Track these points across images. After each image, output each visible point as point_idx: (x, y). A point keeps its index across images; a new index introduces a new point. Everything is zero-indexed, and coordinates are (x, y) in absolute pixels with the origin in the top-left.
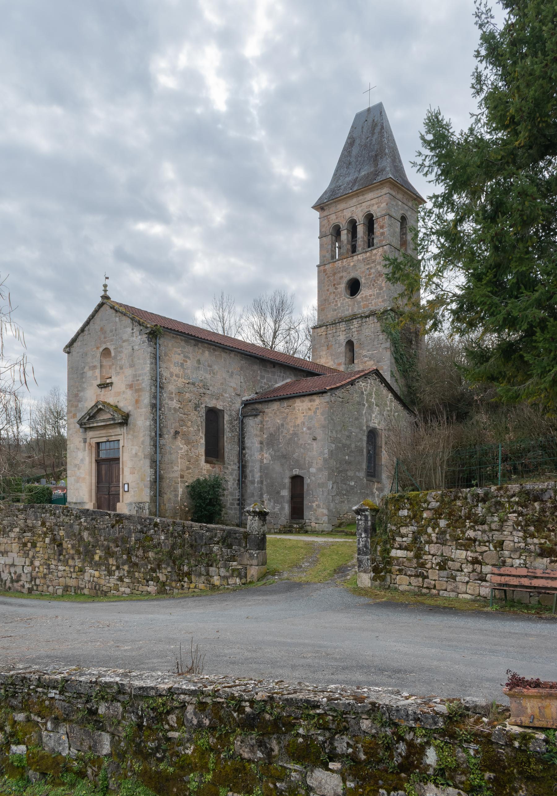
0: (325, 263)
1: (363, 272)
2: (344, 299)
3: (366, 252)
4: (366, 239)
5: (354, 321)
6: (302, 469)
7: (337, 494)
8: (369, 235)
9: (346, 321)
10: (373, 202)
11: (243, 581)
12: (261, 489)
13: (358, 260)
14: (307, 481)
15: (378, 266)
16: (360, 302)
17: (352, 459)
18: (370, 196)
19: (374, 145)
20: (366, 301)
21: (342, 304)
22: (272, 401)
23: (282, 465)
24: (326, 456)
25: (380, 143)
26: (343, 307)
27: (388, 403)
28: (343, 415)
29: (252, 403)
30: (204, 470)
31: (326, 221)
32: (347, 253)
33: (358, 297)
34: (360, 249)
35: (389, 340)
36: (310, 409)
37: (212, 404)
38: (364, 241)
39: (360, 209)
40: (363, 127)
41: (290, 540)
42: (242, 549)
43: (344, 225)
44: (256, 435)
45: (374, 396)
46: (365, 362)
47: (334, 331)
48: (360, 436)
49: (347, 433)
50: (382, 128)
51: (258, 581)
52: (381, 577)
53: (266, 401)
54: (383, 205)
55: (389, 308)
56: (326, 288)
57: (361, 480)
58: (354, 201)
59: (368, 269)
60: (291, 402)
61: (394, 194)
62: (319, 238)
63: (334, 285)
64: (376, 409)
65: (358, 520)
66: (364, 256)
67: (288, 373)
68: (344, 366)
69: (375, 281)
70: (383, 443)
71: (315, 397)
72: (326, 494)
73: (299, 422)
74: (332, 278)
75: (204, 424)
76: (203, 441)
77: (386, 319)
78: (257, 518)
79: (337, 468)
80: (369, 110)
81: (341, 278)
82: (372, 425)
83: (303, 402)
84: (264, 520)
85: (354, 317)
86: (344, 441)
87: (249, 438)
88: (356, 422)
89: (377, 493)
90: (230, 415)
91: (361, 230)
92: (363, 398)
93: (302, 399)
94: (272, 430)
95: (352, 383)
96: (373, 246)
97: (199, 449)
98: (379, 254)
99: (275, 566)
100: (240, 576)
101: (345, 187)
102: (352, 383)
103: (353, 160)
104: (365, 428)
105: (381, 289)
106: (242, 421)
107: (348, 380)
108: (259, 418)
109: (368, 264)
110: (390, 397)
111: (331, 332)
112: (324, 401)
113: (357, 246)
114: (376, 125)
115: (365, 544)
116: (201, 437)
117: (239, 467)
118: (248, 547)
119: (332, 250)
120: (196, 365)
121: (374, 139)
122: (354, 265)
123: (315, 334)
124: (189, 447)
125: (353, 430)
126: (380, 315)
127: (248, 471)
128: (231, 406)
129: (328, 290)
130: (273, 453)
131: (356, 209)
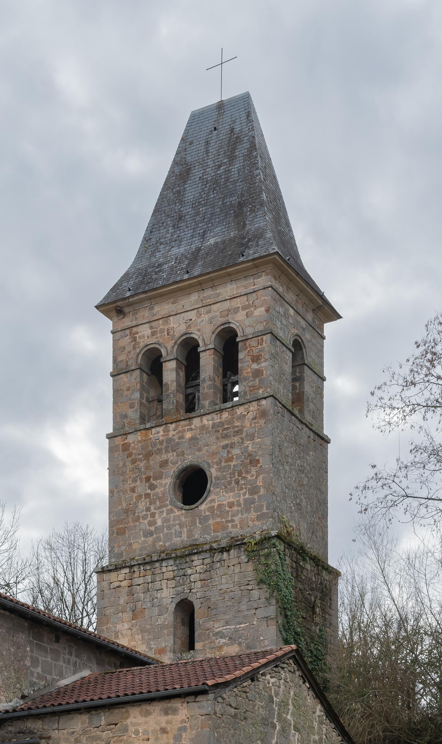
0: (127, 429)
1: (214, 454)
2: (171, 511)
3: (221, 410)
4: (218, 383)
5: (195, 557)
8: (224, 376)
9: (176, 558)
10: (237, 303)
13: (203, 427)
15: (247, 443)
16: (206, 519)
18: (229, 289)
19: (235, 182)
20: (221, 516)
21: (166, 520)
22: (68, 712)
26: (169, 528)
27: (316, 725)
29: (19, 718)
31: (128, 339)
32: (177, 410)
33: (203, 507)
34: (206, 403)
35: (274, 601)
36: (164, 731)
38: (215, 387)
39: (206, 317)
43: (169, 349)
45: (291, 707)
46: (220, 648)
50: (253, 147)
53: (53, 714)
54: (260, 311)
55: (274, 533)
56: (130, 484)
59: (224, 447)
61: (281, 290)
63: (148, 479)
66: (217, 419)
67: (85, 657)
68: (171, 655)
71: (176, 704)
74: (142, 464)
77: (267, 556)
80: (221, 106)
83: (148, 714)
85: (193, 550)
91: (208, 363)
93: (146, 707)
95: (253, 676)
98: (250, 416)
101: (172, 268)
102: (253, 676)
103: (188, 210)
105: (254, 490)
107: (246, 669)
109: (226, 437)
110: (318, 713)
111: (141, 581)
112: (198, 711)
122: (193, 439)
123: (105, 584)
126: (254, 548)
129: (133, 490)
131: (194, 318)
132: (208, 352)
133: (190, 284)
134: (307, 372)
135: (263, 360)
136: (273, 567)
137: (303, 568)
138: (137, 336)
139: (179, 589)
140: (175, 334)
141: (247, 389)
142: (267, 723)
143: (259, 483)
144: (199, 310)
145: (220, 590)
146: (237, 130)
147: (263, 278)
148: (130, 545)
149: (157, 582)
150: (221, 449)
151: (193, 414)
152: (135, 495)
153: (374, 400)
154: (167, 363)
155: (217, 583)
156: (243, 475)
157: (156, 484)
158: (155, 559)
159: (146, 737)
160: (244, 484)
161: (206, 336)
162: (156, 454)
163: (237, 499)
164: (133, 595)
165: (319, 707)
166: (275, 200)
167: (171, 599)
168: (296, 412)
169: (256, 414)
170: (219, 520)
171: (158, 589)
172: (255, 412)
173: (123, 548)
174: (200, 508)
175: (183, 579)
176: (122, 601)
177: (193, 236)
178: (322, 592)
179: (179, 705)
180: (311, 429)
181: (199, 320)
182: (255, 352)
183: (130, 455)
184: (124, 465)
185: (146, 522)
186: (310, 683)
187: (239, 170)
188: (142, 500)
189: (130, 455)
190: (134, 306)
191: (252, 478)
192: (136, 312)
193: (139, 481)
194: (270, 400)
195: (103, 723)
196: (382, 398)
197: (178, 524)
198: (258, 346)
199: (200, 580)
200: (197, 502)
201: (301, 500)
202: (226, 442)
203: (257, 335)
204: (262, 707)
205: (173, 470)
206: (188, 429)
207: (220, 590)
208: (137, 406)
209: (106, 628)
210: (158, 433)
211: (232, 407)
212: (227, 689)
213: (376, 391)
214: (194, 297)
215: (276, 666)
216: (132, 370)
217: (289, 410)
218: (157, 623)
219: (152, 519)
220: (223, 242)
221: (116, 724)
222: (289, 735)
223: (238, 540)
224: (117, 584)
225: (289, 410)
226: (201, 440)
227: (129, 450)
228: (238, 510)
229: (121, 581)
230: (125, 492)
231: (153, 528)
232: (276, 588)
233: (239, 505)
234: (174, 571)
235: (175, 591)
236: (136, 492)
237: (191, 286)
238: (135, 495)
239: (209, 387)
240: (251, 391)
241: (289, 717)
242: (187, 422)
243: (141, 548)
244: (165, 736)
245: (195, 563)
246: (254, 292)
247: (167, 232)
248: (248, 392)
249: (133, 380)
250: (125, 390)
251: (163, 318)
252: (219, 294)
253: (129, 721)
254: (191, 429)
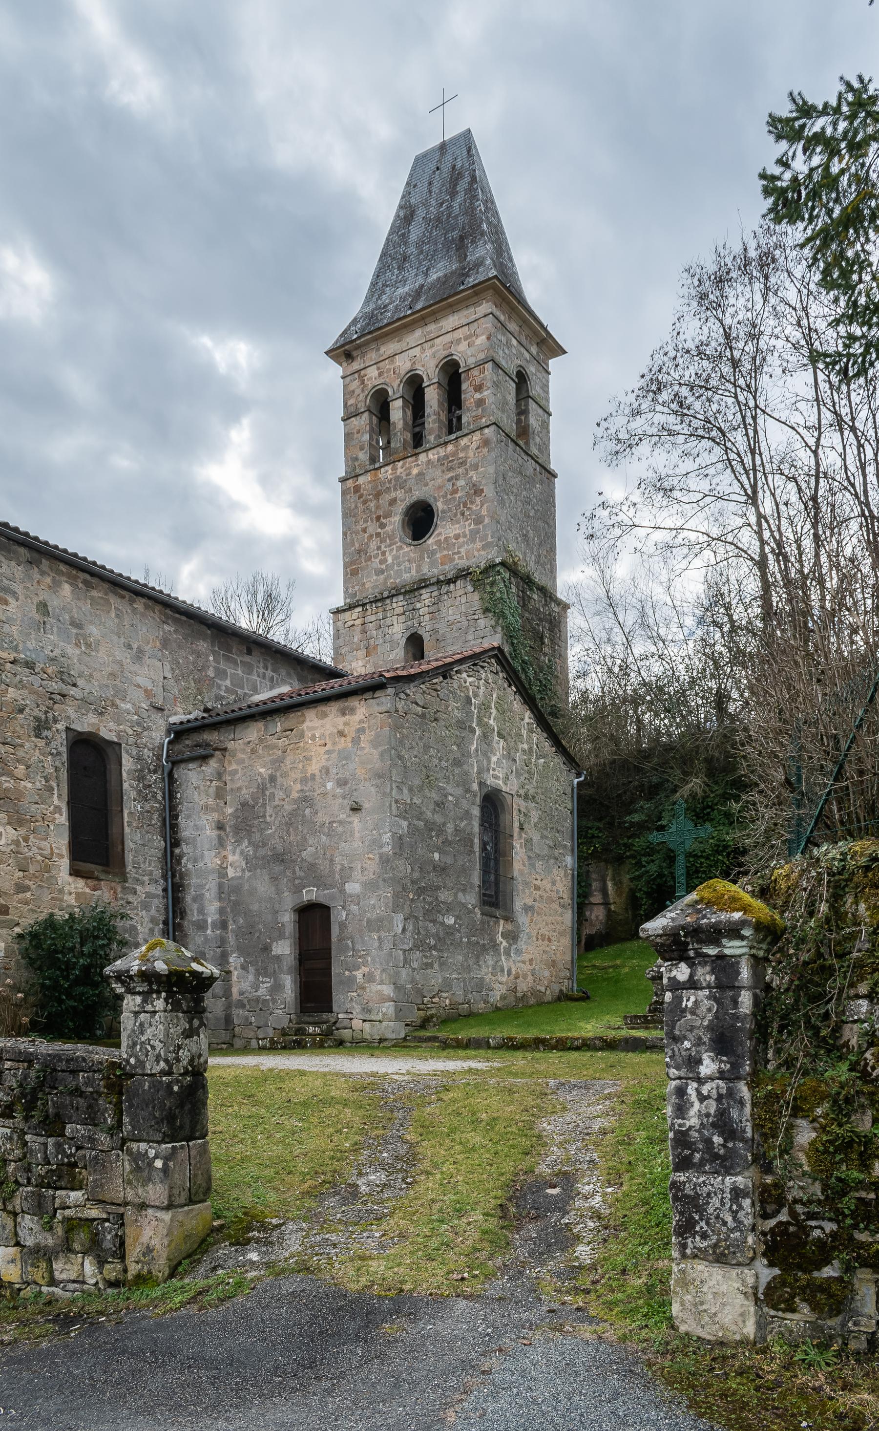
1: (440, 487)
2: (401, 548)
3: (446, 443)
4: (444, 417)
5: (423, 591)
6: (326, 887)
7: (416, 947)
8: (450, 411)
9: (405, 593)
10: (459, 334)
11: (112, 1271)
12: (223, 941)
14: (339, 915)
15: (471, 473)
16: (434, 552)
17: (449, 860)
18: (451, 321)
19: (456, 216)
20: (448, 549)
21: (396, 558)
23: (274, 879)
24: (387, 849)
25: (470, 211)
26: (399, 565)
27: (525, 733)
28: (427, 748)
30: (70, 893)
31: (357, 383)
32: (405, 448)
34: (432, 438)
35: (499, 629)
36: (341, 734)
37: (86, 723)
38: (440, 421)
39: (429, 352)
40: (430, 184)
41: (302, 1073)
42: (103, 1138)
43: (395, 388)
44: (206, 808)
45: (494, 711)
47: (380, 615)
48: (465, 804)
49: (435, 796)
50: (474, 179)
51: (172, 1275)
52: (824, 1287)
55: (498, 560)
56: (362, 525)
57: (470, 912)
58: (418, 335)
59: (449, 480)
60: (292, 719)
61: (502, 318)
62: (344, 420)
63: (378, 518)
64: (499, 745)
65: (676, 986)
66: (441, 452)
70: (516, 825)
71: (353, 702)
72: (387, 946)
73: (314, 768)
75: (64, 775)
76: (63, 819)
77: (492, 584)
78: (160, 1004)
79: (414, 882)
80: (443, 147)
81: (393, 502)
82: (490, 781)
83: (324, 715)
84: (196, 1011)
85: (422, 584)
86: (429, 814)
87: (188, 817)
88: (457, 771)
89: (505, 944)
90: (139, 759)
91: (432, 397)
92: (469, 713)
93: (322, 708)
94: (246, 794)
96: (459, 428)
97: (52, 839)
98: (474, 446)
99: (247, 1198)
100: (94, 1248)
101: (396, 307)
103: (413, 250)
104: (475, 787)
105: (479, 521)
106: (171, 774)
108: (213, 763)
109: (451, 469)
110: (527, 720)
111: (373, 618)
113: (426, 432)
114: (460, 175)
115: (722, 1114)
116: (58, 809)
117: (165, 890)
118: (127, 1128)
119: (371, 445)
120: (37, 617)
121: (456, 205)
122: (421, 474)
123: (340, 624)
124: (23, 831)
125: (449, 789)
126: (479, 577)
127: (188, 899)
128: (138, 735)
130: (250, 851)
131: (418, 355)
134: (532, 405)
136: (498, 595)
137: (530, 598)
139: (409, 623)
142: (463, 725)
146: (459, 165)
148: (363, 584)
151: (419, 450)
152: (366, 535)
153: (600, 431)
159: (323, 742)
161: (430, 372)
165: (528, 714)
166: (497, 233)
168: (521, 443)
170: (445, 553)
173: (357, 588)
176: (356, 640)
177: (417, 275)
178: (551, 622)
179: (356, 703)
180: (537, 462)
181: (423, 356)
182: (478, 381)
183: (360, 497)
184: (356, 507)
186: (516, 687)
187: (460, 205)
189: (360, 497)
192: (363, 354)
194: (493, 427)
195: (279, 729)
196: (607, 428)
201: (528, 532)
202: (451, 474)
204: (457, 708)
208: (367, 448)
212: (412, 685)
213: (602, 422)
214: (418, 333)
215: (474, 665)
217: (512, 440)
220: (445, 276)
221: (292, 730)
222: (492, 741)
224: (351, 623)
225: (512, 440)
230: (357, 533)
231: (384, 567)
232: (501, 615)
233: (465, 536)
237: (414, 322)
238: (366, 535)
239: (434, 421)
241: (491, 722)
242: (413, 459)
244: (343, 739)
245: (423, 597)
247: (393, 274)
253: (305, 726)
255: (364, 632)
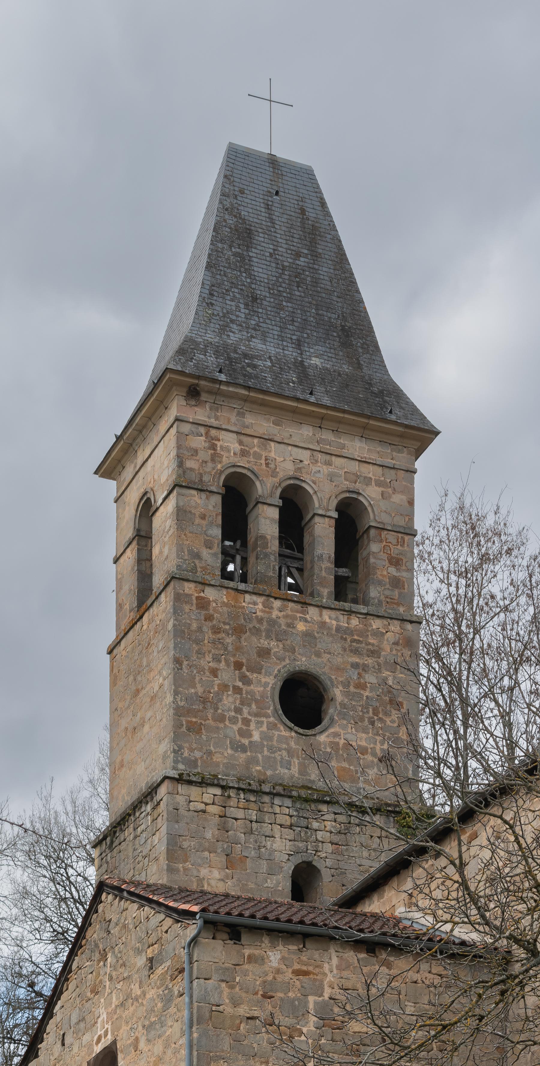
13: (323, 625)
21: (265, 736)
26: (270, 749)
33: (322, 738)
59: (355, 666)
69: (376, 713)
109: (356, 652)
122: (307, 635)
123: (181, 800)
132: (327, 519)
133: (313, 411)
135: (404, 568)
138: (219, 444)
140: (278, 470)
141: (382, 598)
143: (403, 735)
144: (315, 453)
145: (360, 866)
147: (404, 455)
149: (266, 825)
150: (349, 667)
152: (217, 681)
154: (265, 507)
155: (356, 855)
156: (381, 716)
157: (251, 677)
158: (266, 788)
160: (381, 728)
162: (253, 634)
163: (372, 746)
164: (227, 831)
167: (287, 857)
169: (399, 639)
170: (345, 765)
171: (267, 834)
172: (397, 635)
174: (317, 737)
175: (306, 833)
184: (200, 629)
185: (235, 728)
188: (230, 693)
190: (218, 397)
191: (391, 724)
193: (223, 663)
197: (285, 749)
198: (397, 545)
199: (332, 844)
200: (302, 728)
203: (398, 530)
205: (279, 667)
206: (300, 617)
207: (360, 866)
209: (183, 867)
210: (255, 603)
211: (367, 614)
216: (211, 492)
218: (266, 885)
219: (244, 728)
223: (389, 805)
226: (320, 642)
227: (207, 609)
228: (373, 762)
229: (206, 804)
230: (201, 670)
234: (291, 816)
235: (294, 845)
236: (220, 677)
237: (310, 415)
238: (217, 681)
240: (387, 602)
242: (298, 607)
243: (227, 763)
246: (394, 468)
248: (384, 603)
249: (211, 507)
250: (197, 516)
251: (260, 438)
252: (343, 447)
254: (306, 621)
255: (225, 829)
